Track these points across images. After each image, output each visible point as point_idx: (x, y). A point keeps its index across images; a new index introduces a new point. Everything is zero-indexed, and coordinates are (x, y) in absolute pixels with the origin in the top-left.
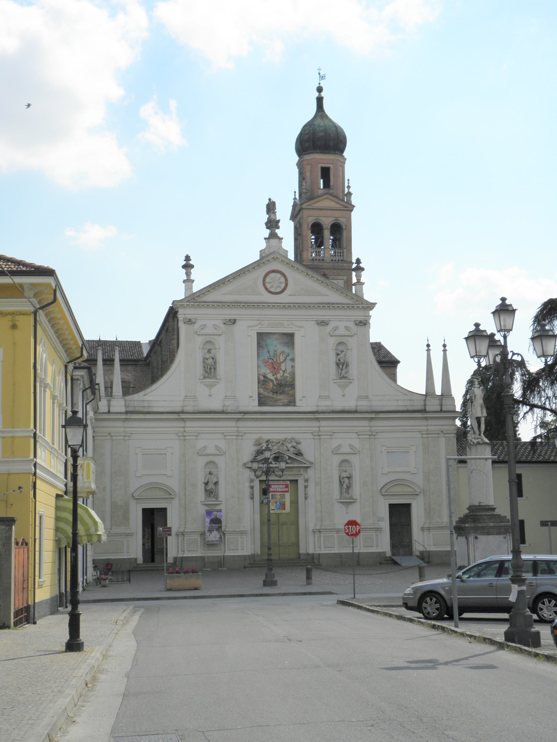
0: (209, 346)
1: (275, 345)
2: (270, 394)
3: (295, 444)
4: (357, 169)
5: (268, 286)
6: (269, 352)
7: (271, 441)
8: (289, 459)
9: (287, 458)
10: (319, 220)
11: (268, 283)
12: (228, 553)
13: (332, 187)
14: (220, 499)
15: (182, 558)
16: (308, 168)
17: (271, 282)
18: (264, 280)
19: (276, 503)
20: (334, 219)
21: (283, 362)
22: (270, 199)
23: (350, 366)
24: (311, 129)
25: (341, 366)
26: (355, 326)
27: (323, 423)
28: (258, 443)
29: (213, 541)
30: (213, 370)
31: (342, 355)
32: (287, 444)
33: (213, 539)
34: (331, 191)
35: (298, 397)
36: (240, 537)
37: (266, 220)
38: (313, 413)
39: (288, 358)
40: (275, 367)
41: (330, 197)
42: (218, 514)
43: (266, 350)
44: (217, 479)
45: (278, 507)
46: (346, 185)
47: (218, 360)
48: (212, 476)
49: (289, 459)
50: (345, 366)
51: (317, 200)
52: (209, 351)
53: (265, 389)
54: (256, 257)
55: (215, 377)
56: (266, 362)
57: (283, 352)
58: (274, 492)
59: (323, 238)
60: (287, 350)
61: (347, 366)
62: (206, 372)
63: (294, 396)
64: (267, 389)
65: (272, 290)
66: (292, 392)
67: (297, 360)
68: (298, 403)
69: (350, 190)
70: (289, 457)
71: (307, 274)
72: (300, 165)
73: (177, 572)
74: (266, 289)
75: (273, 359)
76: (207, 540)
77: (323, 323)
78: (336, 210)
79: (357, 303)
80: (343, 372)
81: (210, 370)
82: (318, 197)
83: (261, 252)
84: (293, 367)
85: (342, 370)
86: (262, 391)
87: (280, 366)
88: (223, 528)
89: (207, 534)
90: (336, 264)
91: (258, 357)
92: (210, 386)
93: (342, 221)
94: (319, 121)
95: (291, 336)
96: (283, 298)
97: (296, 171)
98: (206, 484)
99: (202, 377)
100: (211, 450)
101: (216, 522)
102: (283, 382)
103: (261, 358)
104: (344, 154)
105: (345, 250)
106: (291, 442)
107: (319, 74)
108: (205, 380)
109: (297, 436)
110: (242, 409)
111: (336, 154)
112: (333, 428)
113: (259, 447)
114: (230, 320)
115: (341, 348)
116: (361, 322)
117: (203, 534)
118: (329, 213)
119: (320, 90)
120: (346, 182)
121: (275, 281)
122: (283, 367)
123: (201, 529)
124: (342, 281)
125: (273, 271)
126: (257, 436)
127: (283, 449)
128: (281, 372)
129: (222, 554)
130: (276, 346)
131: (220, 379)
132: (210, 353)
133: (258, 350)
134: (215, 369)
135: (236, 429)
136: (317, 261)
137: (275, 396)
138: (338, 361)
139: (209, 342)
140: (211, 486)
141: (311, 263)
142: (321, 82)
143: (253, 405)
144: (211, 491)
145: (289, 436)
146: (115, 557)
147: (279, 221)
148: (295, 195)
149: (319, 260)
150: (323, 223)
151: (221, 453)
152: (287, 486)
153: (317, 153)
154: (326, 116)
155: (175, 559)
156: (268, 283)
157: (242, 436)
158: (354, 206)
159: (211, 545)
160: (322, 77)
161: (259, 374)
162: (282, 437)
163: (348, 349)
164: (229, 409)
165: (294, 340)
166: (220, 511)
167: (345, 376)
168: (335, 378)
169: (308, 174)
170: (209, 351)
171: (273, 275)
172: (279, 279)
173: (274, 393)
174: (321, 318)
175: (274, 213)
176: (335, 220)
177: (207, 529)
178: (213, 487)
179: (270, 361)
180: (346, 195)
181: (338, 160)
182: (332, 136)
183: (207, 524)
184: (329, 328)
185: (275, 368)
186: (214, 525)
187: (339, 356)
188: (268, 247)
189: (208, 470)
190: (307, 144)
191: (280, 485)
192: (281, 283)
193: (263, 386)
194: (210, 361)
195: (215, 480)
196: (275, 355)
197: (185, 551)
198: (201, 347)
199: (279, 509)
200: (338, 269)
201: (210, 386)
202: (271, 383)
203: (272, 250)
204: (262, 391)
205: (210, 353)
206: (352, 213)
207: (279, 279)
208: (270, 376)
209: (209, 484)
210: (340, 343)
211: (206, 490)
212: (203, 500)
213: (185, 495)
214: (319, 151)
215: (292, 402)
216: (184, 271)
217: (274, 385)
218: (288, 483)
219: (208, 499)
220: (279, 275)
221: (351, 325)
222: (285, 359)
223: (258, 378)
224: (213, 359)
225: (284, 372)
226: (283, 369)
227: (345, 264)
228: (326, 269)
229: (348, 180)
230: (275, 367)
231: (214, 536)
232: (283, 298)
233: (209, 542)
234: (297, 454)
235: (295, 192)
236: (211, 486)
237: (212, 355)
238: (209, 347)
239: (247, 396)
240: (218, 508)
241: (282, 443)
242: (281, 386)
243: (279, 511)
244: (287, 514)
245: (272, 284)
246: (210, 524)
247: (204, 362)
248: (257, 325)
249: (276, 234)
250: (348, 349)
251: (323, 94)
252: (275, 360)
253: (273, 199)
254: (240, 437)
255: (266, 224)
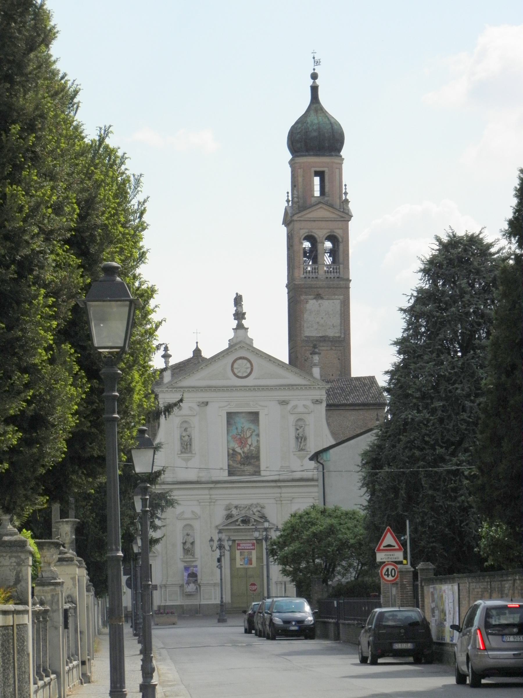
0: (185, 425)
1: (242, 423)
2: (239, 466)
3: (259, 509)
4: (357, 171)
5: (236, 371)
6: (237, 429)
7: (297, 435)
8: (255, 522)
9: (253, 520)
10: (312, 232)
11: (236, 368)
12: (203, 602)
13: (327, 194)
14: (196, 557)
15: (165, 606)
16: (300, 172)
17: (239, 368)
18: (232, 370)
19: (244, 559)
20: (329, 231)
21: (249, 437)
22: (237, 294)
23: (308, 440)
24: (303, 127)
25: (300, 440)
26: (312, 404)
27: (284, 490)
28: (228, 508)
29: (191, 592)
30: (189, 446)
31: (301, 430)
32: (253, 509)
33: (191, 590)
34: (326, 199)
35: (263, 467)
36: (213, 588)
37: (234, 312)
38: (275, 481)
39: (254, 434)
40: (242, 442)
41: (324, 206)
42: (194, 569)
43: (234, 427)
44: (194, 539)
45: (246, 562)
46: (344, 191)
47: (193, 437)
48: (189, 537)
49: (255, 522)
50: (303, 440)
51: (310, 210)
52: (186, 430)
53: (234, 461)
54: (225, 346)
55: (191, 452)
56: (234, 438)
57: (249, 429)
58: (243, 549)
59: (317, 251)
60: (252, 427)
61: (305, 439)
62: (184, 448)
63: (259, 466)
64: (236, 461)
65: (240, 374)
66: (257, 463)
67: (261, 435)
68: (262, 473)
69: (348, 197)
70: (254, 519)
71: (270, 360)
72: (292, 163)
73: (161, 613)
74: (235, 374)
75: (240, 435)
76: (185, 591)
77: (284, 403)
78: (331, 221)
79: (314, 384)
80: (302, 445)
81: (186, 446)
82: (312, 206)
83: (229, 341)
84: (258, 441)
85: (301, 443)
86: (231, 463)
87: (247, 441)
88: (199, 581)
89: (186, 586)
90: (331, 283)
91: (228, 433)
92: (187, 460)
93: (338, 233)
94: (313, 118)
95: (256, 415)
96: (249, 381)
97: (289, 170)
98: (184, 543)
99: (180, 452)
100: (188, 515)
101: (193, 576)
102: (249, 455)
103: (231, 434)
104: (342, 153)
105: (341, 266)
106: (257, 507)
107: (314, 58)
108: (182, 455)
109: (261, 502)
110: (214, 479)
111: (332, 156)
112: (293, 495)
113: (229, 512)
114: (203, 402)
115: (300, 423)
116: (317, 401)
117: (182, 586)
118: (323, 224)
119: (314, 76)
120: (344, 187)
121: (242, 367)
122: (249, 442)
123: (181, 582)
124: (339, 301)
125: (241, 358)
126: (227, 502)
127: (249, 513)
128: (248, 446)
129: (198, 603)
130: (243, 423)
131: (195, 454)
132: (187, 431)
133: (227, 427)
134: (190, 445)
135: (209, 496)
136: (310, 280)
137: (242, 467)
138: (297, 435)
139: (185, 422)
140: (188, 545)
141: (303, 282)
142: (316, 67)
143: (224, 475)
144: (188, 549)
145: (255, 502)
146: (190, 603)
147: (244, 314)
148: (288, 196)
149: (313, 278)
150: (316, 236)
151: (197, 517)
152: (253, 545)
153: (310, 155)
154: (322, 109)
155: (159, 607)
156: (236, 368)
157: (214, 502)
158: (352, 216)
159: (189, 595)
160: (317, 63)
161: (228, 448)
162: (249, 502)
163: (305, 425)
164: (203, 479)
165: (258, 418)
166: (196, 567)
167: (304, 448)
168: (295, 450)
169: (300, 179)
170: (186, 430)
171: (240, 361)
172: (246, 365)
173: (241, 464)
174: (283, 398)
175: (241, 306)
176: (331, 232)
177: (185, 582)
178: (190, 546)
179: (238, 436)
180: (342, 202)
181: (333, 163)
182: (327, 135)
183: (186, 578)
184: (289, 407)
185: (242, 443)
186: (191, 579)
187: (298, 431)
188: (236, 336)
189: (185, 532)
190: (299, 145)
191: (247, 543)
192: (247, 368)
193: (232, 459)
194: (187, 438)
195: (191, 540)
196: (242, 431)
197: (167, 599)
198: (179, 426)
199: (247, 564)
200: (334, 288)
201: (187, 460)
202: (239, 456)
203: (239, 340)
204: (231, 463)
205: (187, 431)
206: (349, 222)
207: (246, 365)
208: (238, 450)
209: (187, 543)
210: (300, 420)
211: (184, 548)
212: (182, 557)
213: (166, 553)
214: (312, 153)
215: (257, 472)
216: (163, 360)
217: (242, 458)
218: (255, 542)
219: (185, 557)
220: (245, 362)
221: (309, 403)
222: (251, 435)
223: (228, 452)
224: (189, 436)
225: (250, 446)
226: (250, 443)
227: (341, 282)
228: (320, 288)
229: (345, 185)
230: (242, 442)
231: (191, 588)
232: (249, 381)
233: (186, 592)
234: (261, 517)
235: (288, 193)
236: (188, 545)
237: (188, 433)
238: (185, 426)
239: (218, 465)
240: (194, 564)
241: (249, 507)
242: (247, 459)
243: (246, 566)
244: (255, 568)
245: (239, 369)
246: (188, 577)
247: (181, 439)
248: (226, 406)
249: (243, 325)
250: (305, 425)
251: (318, 81)
252: (242, 435)
253: (240, 293)
254: (213, 504)
255: (234, 315)
